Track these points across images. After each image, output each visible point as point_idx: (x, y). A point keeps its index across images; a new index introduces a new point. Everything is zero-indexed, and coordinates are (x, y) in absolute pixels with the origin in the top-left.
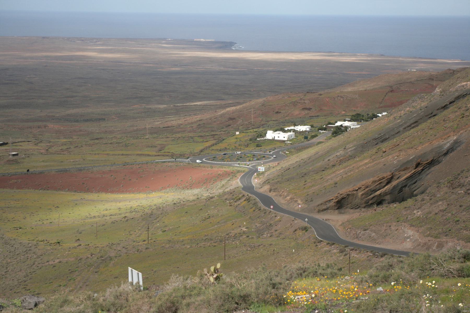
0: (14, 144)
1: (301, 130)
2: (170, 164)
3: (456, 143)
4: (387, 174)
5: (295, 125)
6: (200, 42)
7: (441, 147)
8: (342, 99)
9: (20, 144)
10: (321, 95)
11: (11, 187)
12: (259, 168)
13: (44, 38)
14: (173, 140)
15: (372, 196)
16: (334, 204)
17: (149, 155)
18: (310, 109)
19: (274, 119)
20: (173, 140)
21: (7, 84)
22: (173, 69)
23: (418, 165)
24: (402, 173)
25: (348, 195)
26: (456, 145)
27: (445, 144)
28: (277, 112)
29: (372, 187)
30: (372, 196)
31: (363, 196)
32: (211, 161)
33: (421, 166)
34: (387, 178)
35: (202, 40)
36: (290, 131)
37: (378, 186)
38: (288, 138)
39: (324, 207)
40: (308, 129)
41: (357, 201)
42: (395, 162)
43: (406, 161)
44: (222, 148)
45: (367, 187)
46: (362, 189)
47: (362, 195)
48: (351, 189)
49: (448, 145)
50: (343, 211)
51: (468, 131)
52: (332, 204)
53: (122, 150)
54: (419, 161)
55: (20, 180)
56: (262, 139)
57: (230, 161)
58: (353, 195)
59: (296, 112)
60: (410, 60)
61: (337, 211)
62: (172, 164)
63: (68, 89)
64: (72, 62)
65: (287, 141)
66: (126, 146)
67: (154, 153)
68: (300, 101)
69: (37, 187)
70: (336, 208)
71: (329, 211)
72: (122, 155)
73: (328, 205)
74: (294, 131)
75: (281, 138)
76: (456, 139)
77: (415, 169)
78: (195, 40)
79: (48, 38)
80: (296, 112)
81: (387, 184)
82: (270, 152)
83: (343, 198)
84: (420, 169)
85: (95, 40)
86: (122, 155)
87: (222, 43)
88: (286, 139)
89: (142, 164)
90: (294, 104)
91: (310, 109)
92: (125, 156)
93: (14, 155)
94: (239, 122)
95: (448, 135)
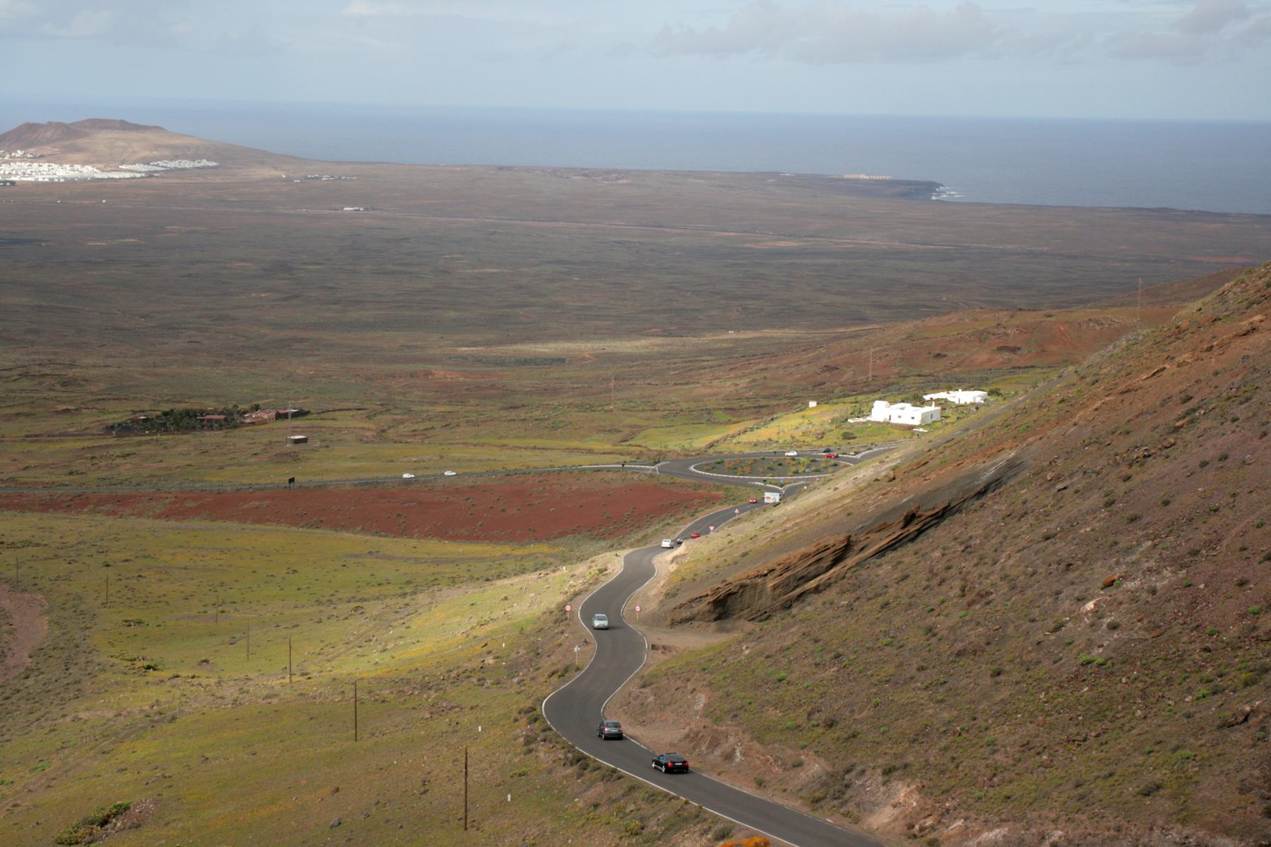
0: (323, 415)
1: (962, 402)
2: (610, 475)
3: (1012, 466)
4: (837, 540)
5: (949, 389)
6: (857, 181)
7: (974, 476)
8: (1098, 328)
9: (332, 415)
10: (1050, 316)
11: (242, 518)
12: (767, 494)
13: (501, 168)
14: (664, 417)
15: (798, 591)
16: (708, 608)
17: (590, 451)
18: (1014, 350)
19: (925, 371)
20: (664, 417)
21: (393, 273)
22: (782, 244)
23: (910, 519)
24: (873, 536)
25: (743, 586)
26: (1010, 473)
27: (985, 470)
28: (938, 355)
29: (800, 570)
30: (798, 591)
31: (778, 591)
32: (707, 471)
33: (916, 521)
34: (832, 549)
35: (863, 176)
36: (929, 403)
37: (812, 568)
38: (922, 420)
39: (685, 614)
40: (978, 400)
41: (765, 602)
42: (872, 508)
43: (891, 507)
44: (762, 439)
45: (787, 569)
46: (777, 573)
47: (775, 587)
48: (752, 573)
49: (992, 471)
50: (729, 626)
51: (1045, 439)
52: (703, 606)
53: (541, 437)
54: (913, 508)
55: (267, 502)
56: (861, 420)
57: (750, 474)
58: (755, 586)
59: (983, 356)
60: (804, 261)
61: (713, 624)
62: (614, 476)
63: (521, 287)
64: (553, 224)
65: (920, 426)
66: (554, 428)
67: (608, 447)
68: (994, 331)
69: (297, 519)
70: (714, 616)
71: (696, 623)
72: (535, 448)
73: (695, 610)
74: (943, 404)
75: (906, 420)
76: (1015, 458)
77: (903, 528)
78: (846, 176)
79: (509, 169)
80: (983, 356)
81: (836, 562)
82: (856, 453)
83: (730, 594)
84: (913, 528)
85: (614, 176)
86: (535, 448)
87: (909, 183)
88: (917, 422)
89: (549, 473)
90: (981, 337)
91: (1014, 350)
92: (538, 452)
93: (297, 441)
94: (846, 377)
95: (1000, 447)
